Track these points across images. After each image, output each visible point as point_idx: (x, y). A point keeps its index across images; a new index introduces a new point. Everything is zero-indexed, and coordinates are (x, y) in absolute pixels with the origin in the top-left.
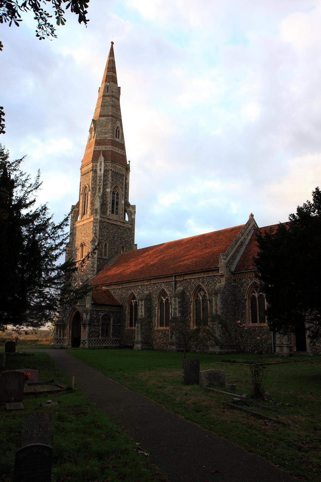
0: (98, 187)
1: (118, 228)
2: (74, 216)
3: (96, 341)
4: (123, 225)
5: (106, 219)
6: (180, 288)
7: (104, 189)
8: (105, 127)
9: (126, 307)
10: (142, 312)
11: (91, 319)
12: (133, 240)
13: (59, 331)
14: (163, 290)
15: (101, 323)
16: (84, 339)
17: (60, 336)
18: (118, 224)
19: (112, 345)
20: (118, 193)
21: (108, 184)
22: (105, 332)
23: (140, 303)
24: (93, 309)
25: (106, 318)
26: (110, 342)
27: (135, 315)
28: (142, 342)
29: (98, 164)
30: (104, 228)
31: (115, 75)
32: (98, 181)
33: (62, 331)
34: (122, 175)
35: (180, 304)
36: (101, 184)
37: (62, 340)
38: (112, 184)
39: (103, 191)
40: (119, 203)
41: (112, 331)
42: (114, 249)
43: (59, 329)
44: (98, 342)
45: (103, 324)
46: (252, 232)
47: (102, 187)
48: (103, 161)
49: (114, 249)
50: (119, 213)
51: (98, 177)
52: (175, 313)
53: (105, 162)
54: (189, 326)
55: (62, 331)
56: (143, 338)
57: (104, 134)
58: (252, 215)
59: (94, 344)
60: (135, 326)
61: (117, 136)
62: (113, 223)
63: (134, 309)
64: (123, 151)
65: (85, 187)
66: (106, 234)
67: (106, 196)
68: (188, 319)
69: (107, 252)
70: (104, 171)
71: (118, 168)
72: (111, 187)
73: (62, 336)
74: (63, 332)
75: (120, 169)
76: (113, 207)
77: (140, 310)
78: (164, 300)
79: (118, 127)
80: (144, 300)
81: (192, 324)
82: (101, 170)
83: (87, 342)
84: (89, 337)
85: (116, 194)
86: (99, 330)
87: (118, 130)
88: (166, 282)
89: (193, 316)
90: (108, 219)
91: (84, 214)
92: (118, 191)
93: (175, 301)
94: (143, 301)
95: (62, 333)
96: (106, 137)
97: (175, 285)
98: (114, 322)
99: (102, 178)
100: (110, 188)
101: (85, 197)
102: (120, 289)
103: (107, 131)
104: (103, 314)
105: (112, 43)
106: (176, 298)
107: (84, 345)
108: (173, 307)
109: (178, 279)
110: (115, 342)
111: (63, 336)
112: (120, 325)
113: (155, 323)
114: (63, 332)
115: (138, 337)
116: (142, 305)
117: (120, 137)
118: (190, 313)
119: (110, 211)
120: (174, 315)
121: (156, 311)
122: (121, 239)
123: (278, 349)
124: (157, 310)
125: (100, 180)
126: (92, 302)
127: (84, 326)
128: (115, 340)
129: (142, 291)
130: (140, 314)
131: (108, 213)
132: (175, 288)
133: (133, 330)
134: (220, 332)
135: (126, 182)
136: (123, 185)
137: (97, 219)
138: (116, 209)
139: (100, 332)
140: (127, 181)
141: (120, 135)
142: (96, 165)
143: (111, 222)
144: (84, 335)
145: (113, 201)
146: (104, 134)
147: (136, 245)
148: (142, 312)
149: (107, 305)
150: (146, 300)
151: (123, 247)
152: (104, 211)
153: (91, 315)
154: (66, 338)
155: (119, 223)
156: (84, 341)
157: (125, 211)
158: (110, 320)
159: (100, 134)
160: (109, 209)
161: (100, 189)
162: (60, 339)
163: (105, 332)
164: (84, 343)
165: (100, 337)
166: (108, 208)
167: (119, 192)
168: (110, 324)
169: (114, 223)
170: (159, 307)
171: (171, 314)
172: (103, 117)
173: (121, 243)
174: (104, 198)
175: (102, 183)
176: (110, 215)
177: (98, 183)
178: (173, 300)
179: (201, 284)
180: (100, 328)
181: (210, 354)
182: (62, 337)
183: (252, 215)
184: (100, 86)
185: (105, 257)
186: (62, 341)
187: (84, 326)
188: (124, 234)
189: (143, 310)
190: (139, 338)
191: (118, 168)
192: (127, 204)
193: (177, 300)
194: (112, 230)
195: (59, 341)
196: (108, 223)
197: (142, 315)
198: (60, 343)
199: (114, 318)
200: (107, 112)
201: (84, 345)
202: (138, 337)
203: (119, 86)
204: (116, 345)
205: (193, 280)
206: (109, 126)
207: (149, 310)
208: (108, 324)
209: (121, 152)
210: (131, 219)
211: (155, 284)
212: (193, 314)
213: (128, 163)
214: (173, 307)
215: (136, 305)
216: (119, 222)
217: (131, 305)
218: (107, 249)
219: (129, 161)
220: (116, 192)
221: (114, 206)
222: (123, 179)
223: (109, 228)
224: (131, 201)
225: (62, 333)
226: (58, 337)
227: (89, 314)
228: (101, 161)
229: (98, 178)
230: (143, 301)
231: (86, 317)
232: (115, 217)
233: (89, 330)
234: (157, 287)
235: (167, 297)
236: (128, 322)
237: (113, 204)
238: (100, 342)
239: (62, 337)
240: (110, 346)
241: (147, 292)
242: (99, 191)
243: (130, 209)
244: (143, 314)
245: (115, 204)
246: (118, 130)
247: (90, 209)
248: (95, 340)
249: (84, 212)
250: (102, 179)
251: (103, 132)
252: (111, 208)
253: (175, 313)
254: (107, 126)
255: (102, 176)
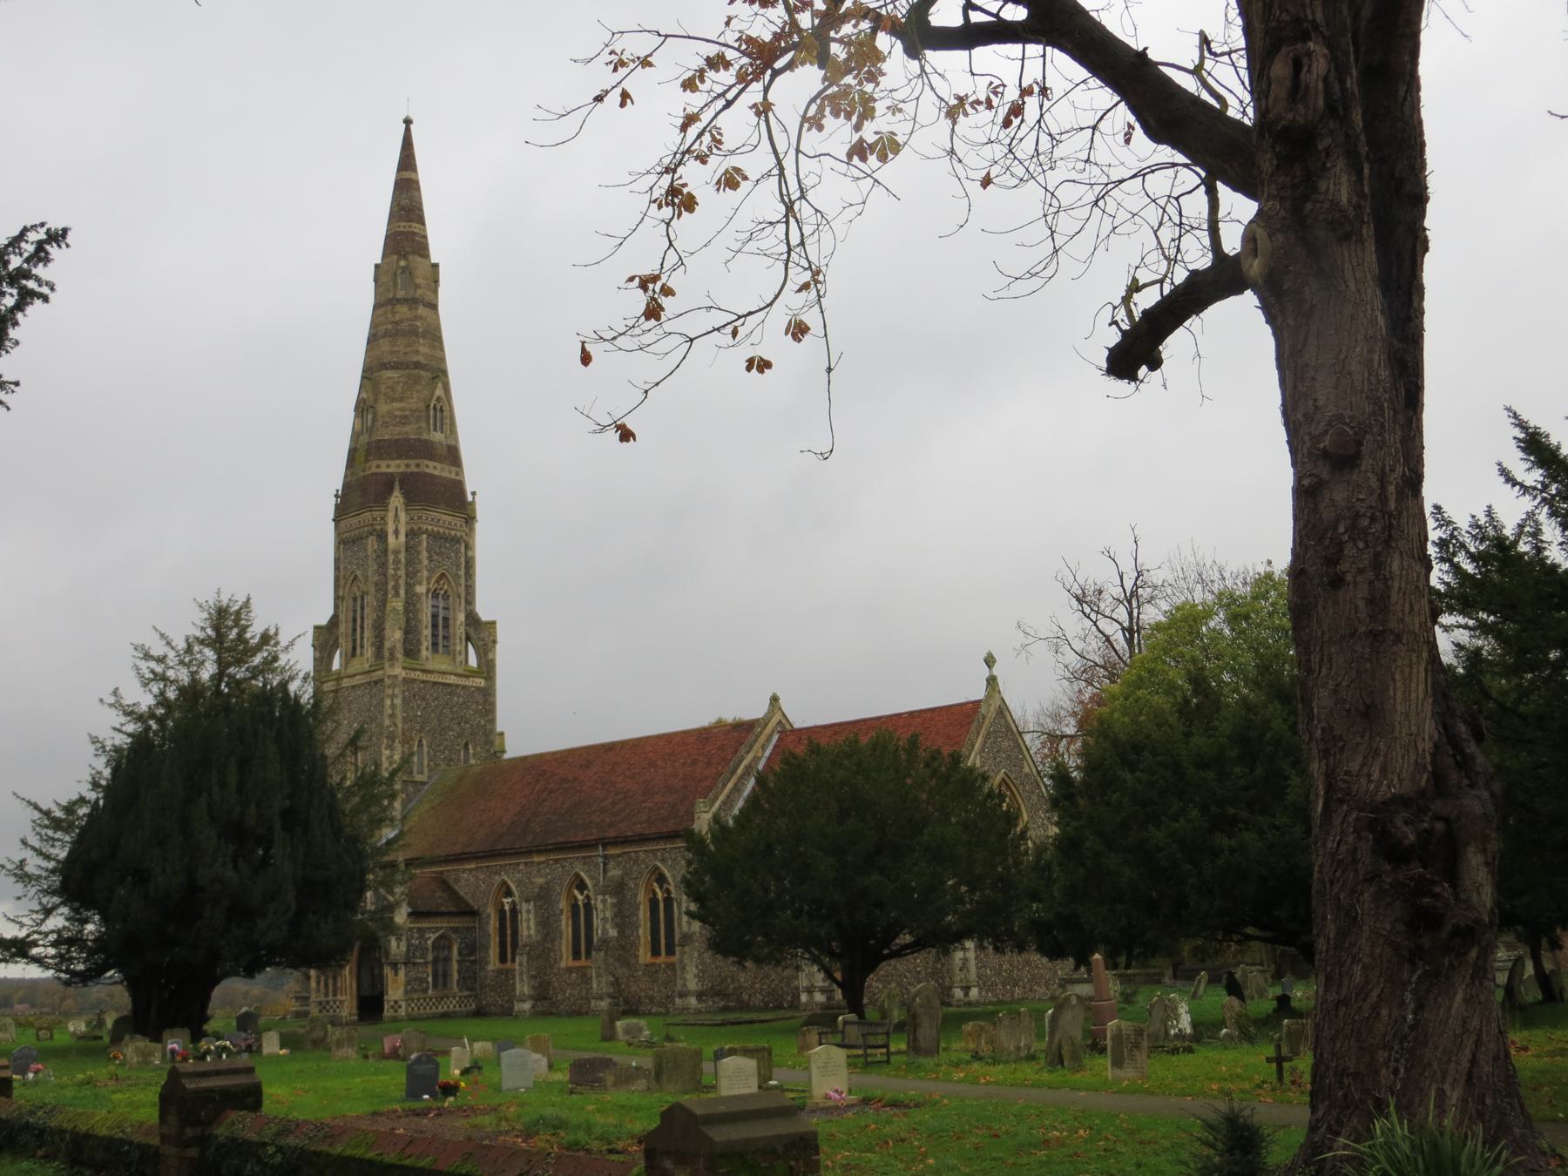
0: (393, 583)
1: (450, 693)
2: (322, 658)
3: (422, 1001)
4: (463, 683)
5: (418, 673)
6: (615, 873)
7: (410, 587)
8: (401, 400)
9: (489, 916)
10: (529, 928)
11: (408, 950)
12: (492, 721)
13: (322, 984)
14: (577, 875)
15: (430, 957)
16: (396, 998)
17: (326, 995)
18: (451, 682)
19: (457, 1008)
20: (446, 592)
21: (419, 571)
22: (441, 979)
23: (525, 907)
24: (412, 925)
25: (442, 944)
26: (454, 1002)
27: (506, 929)
28: (531, 997)
29: (391, 515)
30: (414, 696)
31: (433, 296)
32: (391, 566)
33: (330, 982)
34: (458, 540)
35: (616, 909)
36: (399, 573)
37: (332, 1004)
38: (431, 571)
39: (406, 590)
40: (451, 622)
41: (456, 976)
42: (443, 752)
43: (323, 979)
44: (425, 1004)
45: (435, 961)
46: (776, 737)
47: (402, 582)
48: (403, 507)
49: (443, 752)
50: (451, 648)
51: (390, 553)
52: (604, 930)
53: (407, 510)
54: (637, 957)
55: (330, 982)
56: (534, 987)
57: (400, 422)
58: (775, 699)
59: (416, 1009)
60: (513, 960)
61: (438, 425)
62: (436, 680)
63: (509, 921)
64: (457, 469)
65: (353, 576)
66: (419, 714)
67: (414, 605)
68: (634, 942)
69: (426, 763)
70: (407, 536)
71: (444, 522)
72: (429, 579)
73: (331, 993)
74: (335, 985)
75: (450, 523)
76: (435, 636)
77: (525, 925)
78: (580, 897)
79: (439, 399)
80: (535, 900)
81: (641, 952)
82: (396, 532)
83: (403, 1004)
84: (406, 992)
85: (440, 597)
86: (428, 975)
87: (438, 408)
88: (584, 858)
89: (645, 933)
90: (424, 671)
91: (354, 655)
92: (446, 587)
93: (604, 901)
94: (532, 903)
95: (331, 987)
96: (406, 433)
97: (605, 864)
98: (460, 954)
99: (402, 556)
100: (425, 582)
101: (355, 606)
102: (471, 870)
103: (408, 413)
104: (433, 937)
105: (408, 122)
106: (607, 897)
107: (396, 1011)
108: (601, 915)
109: (612, 851)
110: (466, 1001)
111: (335, 995)
112: (475, 961)
113: (560, 950)
114: (335, 985)
115: (523, 987)
116: (528, 911)
117: (447, 427)
118: (637, 928)
119: (427, 649)
120: (602, 934)
121: (563, 923)
122: (459, 723)
123: (804, 998)
124: (565, 924)
125: (397, 562)
126: (410, 910)
127: (395, 966)
128: (466, 997)
129: (528, 878)
130: (525, 933)
131: (424, 653)
132: (605, 871)
133: (507, 971)
134: (697, 967)
135: (466, 556)
136: (458, 567)
137: (396, 677)
138: (444, 637)
139: (430, 979)
140: (470, 554)
141: (447, 421)
142: (382, 519)
143: (432, 680)
144: (395, 991)
145: (435, 616)
146: (400, 422)
147: (502, 734)
148: (529, 928)
149: (443, 914)
150: (538, 897)
151: (466, 744)
152: (411, 650)
153: (407, 939)
154: (344, 998)
155: (452, 680)
156: (396, 1002)
157: (468, 639)
158: (450, 948)
159: (387, 422)
160: (426, 643)
161: (396, 588)
162: (328, 1003)
163: (441, 979)
164: (396, 1007)
165: (430, 992)
166: (423, 639)
167: (450, 590)
168: (451, 959)
169: (440, 680)
170: (570, 915)
171: (597, 930)
172: (393, 368)
173: (460, 735)
174: (411, 611)
175: (402, 572)
176: (427, 659)
177: (392, 572)
178: (599, 902)
179: (659, 864)
180: (430, 970)
181: (1012, 1085)
182: (330, 997)
183: (775, 699)
184: (379, 262)
185: (419, 778)
186: (331, 1007)
187: (395, 966)
188: (468, 708)
189: (532, 924)
190: (526, 990)
191: (444, 522)
192: (473, 620)
193: (609, 901)
194: (436, 699)
195: (324, 1008)
196: (423, 682)
197: (529, 936)
198: (328, 1011)
199: (461, 943)
200: (405, 353)
201: (396, 1011)
202: (523, 987)
203: (433, 261)
204: (468, 1008)
205: (642, 855)
206: (412, 398)
207: (547, 924)
208: (447, 960)
209: (450, 472)
210: (484, 661)
211: (556, 861)
212: (645, 929)
213: (470, 498)
214: (601, 915)
215: (514, 911)
216: (453, 677)
217: (502, 912)
218: (425, 754)
219: (474, 494)
220: (442, 592)
221: (437, 631)
222: (457, 552)
223: (428, 697)
224: (484, 612)
225: (331, 987)
226: (322, 998)
227: (404, 938)
228: (397, 508)
229: (391, 558)
230: (532, 903)
231: (397, 947)
232: (439, 663)
233: (406, 975)
234: (563, 867)
235: (586, 892)
236: (493, 952)
237: (435, 626)
238: (431, 1004)
239: (330, 997)
240: (455, 1012)
241: (540, 881)
242: (397, 594)
243: (481, 633)
244: (532, 932)
245: (441, 624)
246: (438, 408)
247: (373, 644)
248: (418, 1000)
249: (354, 649)
250: (403, 560)
251: (396, 417)
252: (430, 638)
253: (604, 930)
254: (408, 398)
255: (403, 550)
